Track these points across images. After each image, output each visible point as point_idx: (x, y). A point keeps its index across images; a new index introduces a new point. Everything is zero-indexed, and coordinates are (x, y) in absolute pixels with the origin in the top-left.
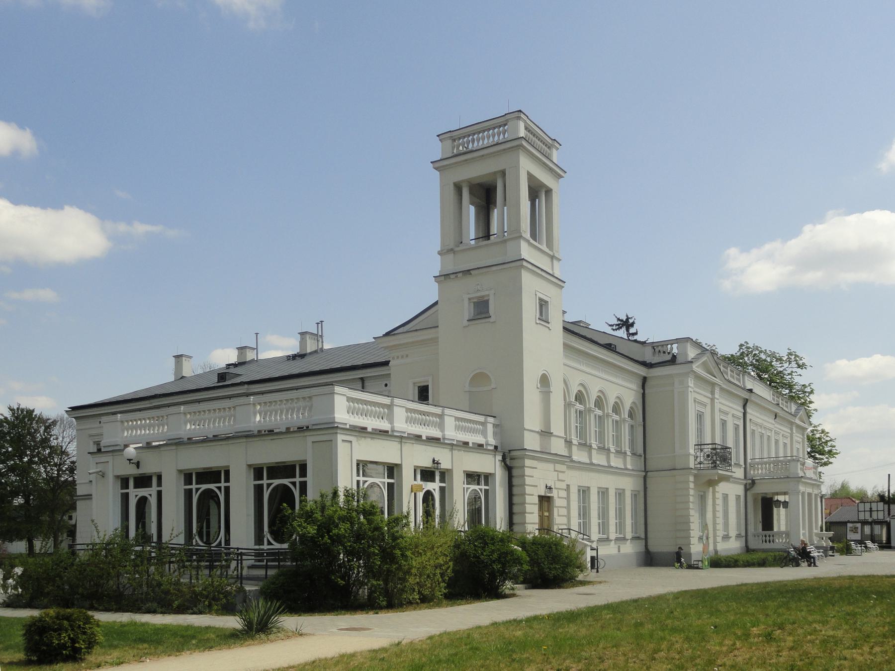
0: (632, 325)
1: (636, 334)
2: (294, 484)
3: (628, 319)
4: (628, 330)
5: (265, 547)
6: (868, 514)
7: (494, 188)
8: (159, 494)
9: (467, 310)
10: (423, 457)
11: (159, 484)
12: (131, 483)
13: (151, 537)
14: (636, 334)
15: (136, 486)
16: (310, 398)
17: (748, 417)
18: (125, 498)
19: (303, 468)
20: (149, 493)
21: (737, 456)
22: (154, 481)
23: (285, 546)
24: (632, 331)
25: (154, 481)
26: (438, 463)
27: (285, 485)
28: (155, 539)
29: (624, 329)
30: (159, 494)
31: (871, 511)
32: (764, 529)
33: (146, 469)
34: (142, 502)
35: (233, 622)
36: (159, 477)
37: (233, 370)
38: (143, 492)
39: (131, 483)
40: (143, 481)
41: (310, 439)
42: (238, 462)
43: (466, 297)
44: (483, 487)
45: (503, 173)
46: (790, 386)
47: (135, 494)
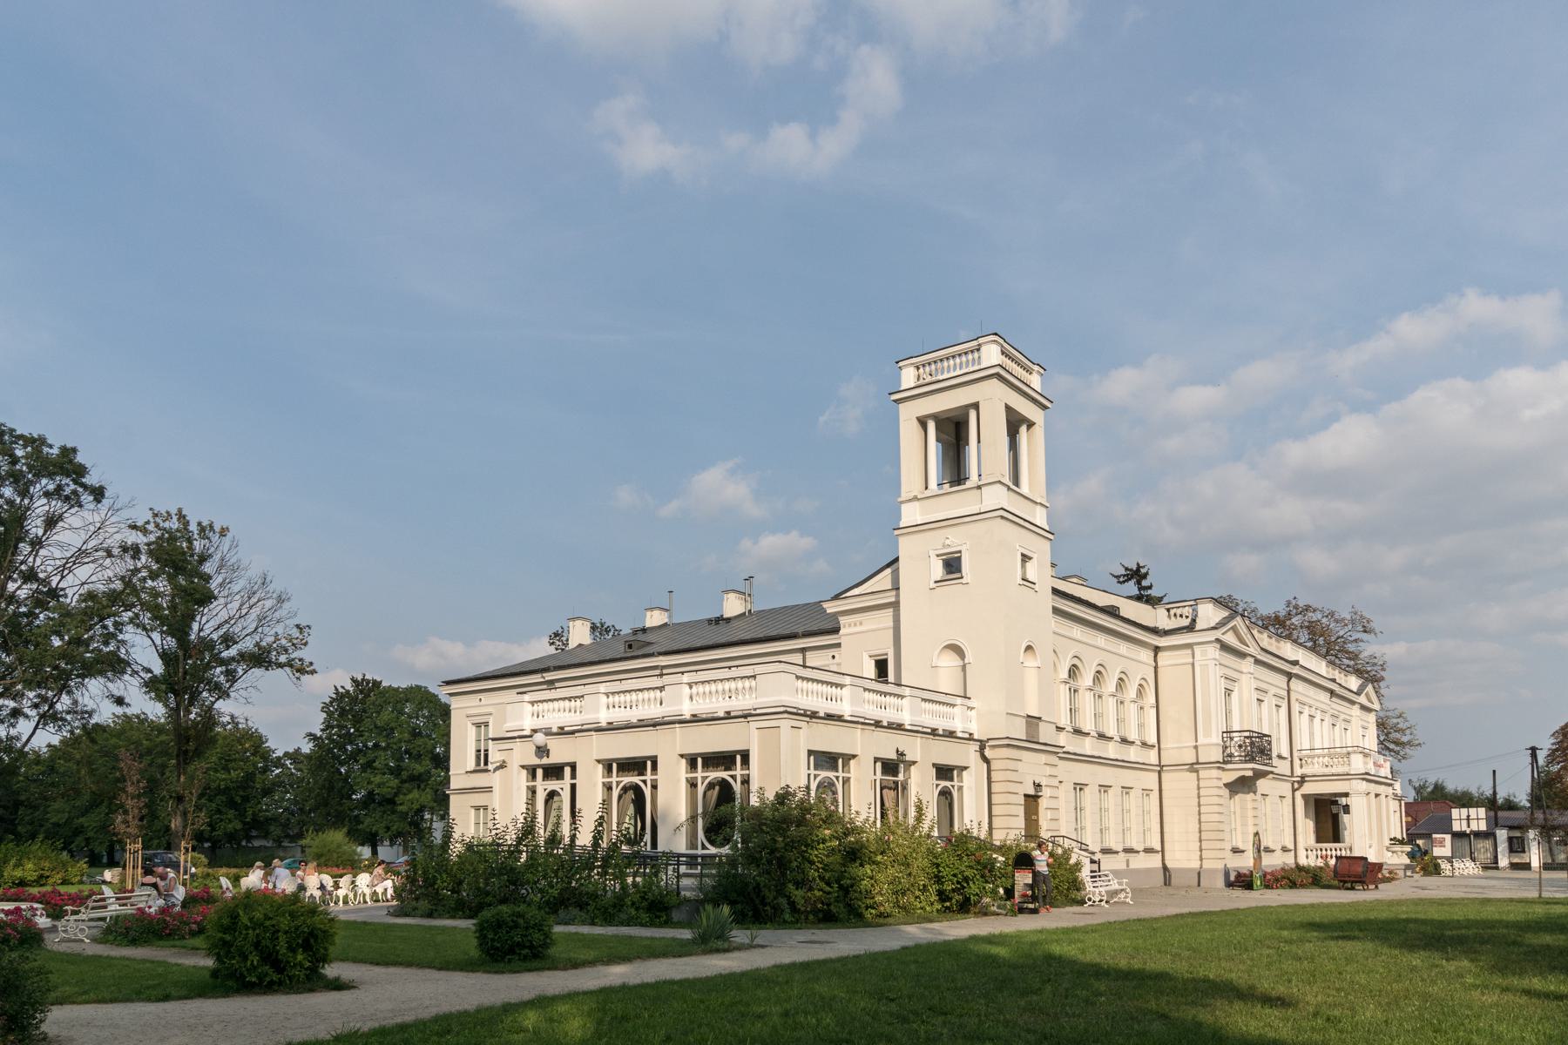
0: (1145, 576)
1: (1150, 587)
2: (704, 778)
3: (1139, 567)
4: (1139, 583)
5: (700, 852)
6: (1464, 823)
7: (967, 422)
8: (573, 787)
9: (938, 570)
10: (887, 746)
11: (573, 776)
12: (540, 772)
13: (562, 838)
14: (1150, 587)
15: (546, 776)
16: (754, 677)
17: (1293, 696)
18: (533, 791)
19: (745, 757)
20: (562, 786)
21: (1280, 746)
22: (567, 770)
23: (726, 850)
24: (1145, 583)
25: (567, 770)
26: (903, 754)
27: (724, 780)
28: (567, 840)
29: (1132, 582)
30: (573, 787)
31: (1468, 819)
32: (1318, 840)
33: (554, 758)
34: (552, 795)
35: (686, 934)
36: (573, 767)
37: (641, 637)
38: (553, 785)
39: (540, 772)
40: (554, 772)
41: (754, 725)
42: (669, 748)
43: (933, 554)
44: (840, 774)
45: (976, 406)
46: (1354, 656)
47: (543, 787)
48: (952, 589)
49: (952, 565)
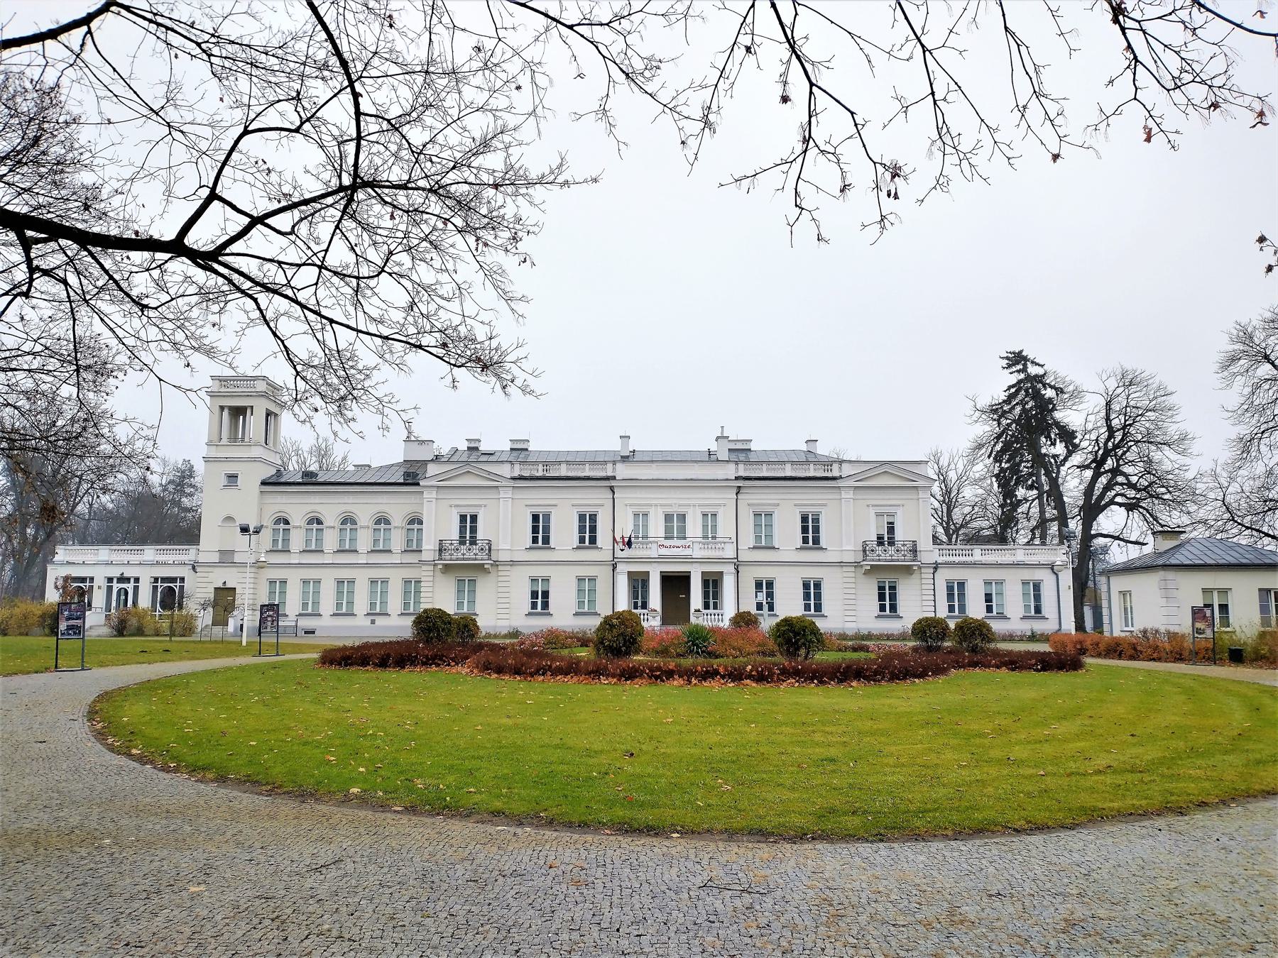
9: (224, 481)
48: (231, 492)
49: (233, 478)
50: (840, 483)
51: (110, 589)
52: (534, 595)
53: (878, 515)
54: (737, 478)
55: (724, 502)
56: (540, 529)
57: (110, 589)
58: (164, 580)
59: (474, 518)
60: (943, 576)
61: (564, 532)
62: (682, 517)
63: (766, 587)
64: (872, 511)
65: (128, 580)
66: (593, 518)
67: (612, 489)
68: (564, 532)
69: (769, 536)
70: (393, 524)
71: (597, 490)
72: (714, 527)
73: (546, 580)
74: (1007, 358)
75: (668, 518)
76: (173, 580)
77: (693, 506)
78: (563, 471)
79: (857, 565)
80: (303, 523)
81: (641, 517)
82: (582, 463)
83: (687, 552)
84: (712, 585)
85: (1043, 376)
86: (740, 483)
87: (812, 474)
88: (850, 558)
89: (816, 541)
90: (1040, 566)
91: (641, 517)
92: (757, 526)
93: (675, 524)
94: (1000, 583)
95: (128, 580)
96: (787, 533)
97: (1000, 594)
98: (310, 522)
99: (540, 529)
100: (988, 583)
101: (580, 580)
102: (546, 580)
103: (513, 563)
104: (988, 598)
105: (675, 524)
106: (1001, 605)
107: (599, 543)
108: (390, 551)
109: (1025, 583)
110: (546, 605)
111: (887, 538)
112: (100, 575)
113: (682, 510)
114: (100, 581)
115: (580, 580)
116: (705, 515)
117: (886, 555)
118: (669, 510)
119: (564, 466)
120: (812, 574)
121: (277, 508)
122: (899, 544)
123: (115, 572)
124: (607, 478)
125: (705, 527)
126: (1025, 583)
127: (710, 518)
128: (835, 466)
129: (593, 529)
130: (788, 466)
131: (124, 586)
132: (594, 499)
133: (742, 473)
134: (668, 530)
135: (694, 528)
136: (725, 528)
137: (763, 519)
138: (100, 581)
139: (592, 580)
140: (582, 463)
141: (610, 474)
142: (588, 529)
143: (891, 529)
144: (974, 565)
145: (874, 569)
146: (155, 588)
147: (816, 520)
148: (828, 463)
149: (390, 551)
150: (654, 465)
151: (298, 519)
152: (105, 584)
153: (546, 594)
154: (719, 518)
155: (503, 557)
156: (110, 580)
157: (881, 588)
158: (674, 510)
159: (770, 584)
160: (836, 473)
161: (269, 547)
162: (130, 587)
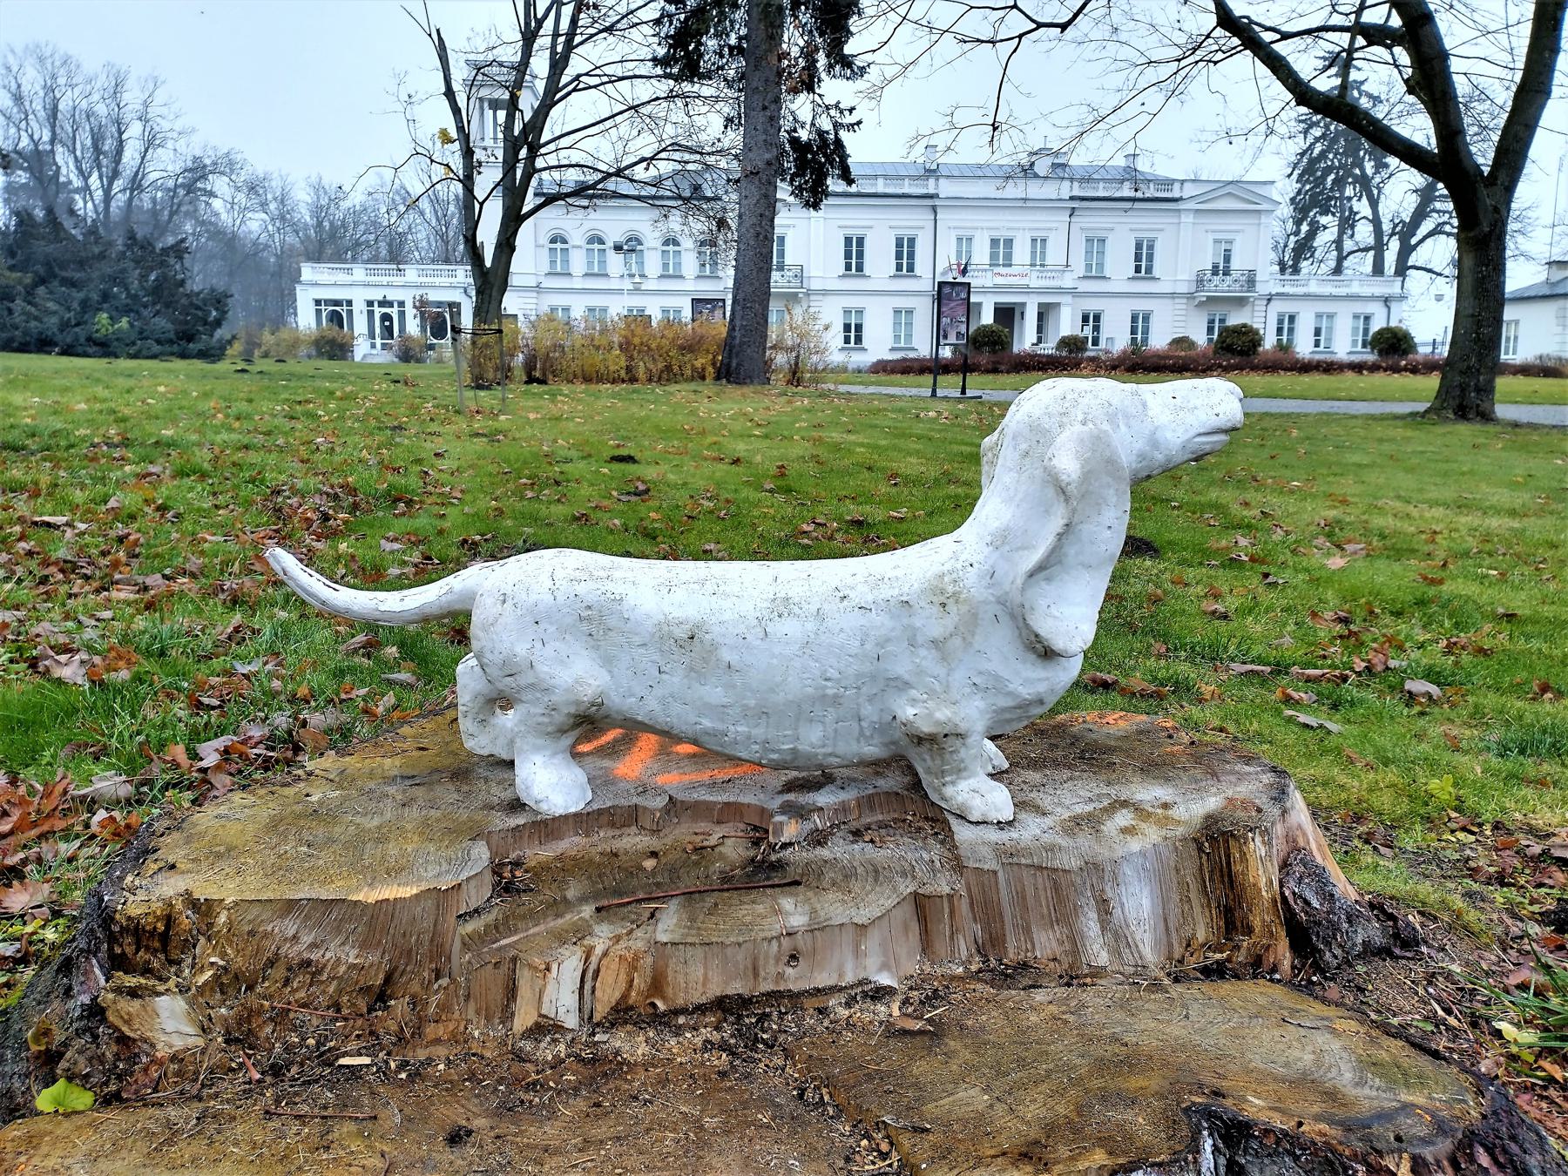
50: (1181, 205)
51: (371, 314)
52: (847, 328)
53: (1217, 241)
54: (1072, 198)
55: (1054, 225)
56: (854, 251)
57: (371, 314)
58: (328, 302)
59: (861, 241)
60: (1277, 307)
61: (880, 259)
62: (1009, 243)
63: (1093, 319)
64: (1211, 237)
65: (390, 304)
66: (912, 241)
67: (934, 209)
68: (880, 259)
69: (1101, 265)
70: (571, 242)
71: (919, 210)
72: (1043, 253)
73: (860, 312)
74: (1325, 59)
75: (994, 242)
76: (337, 303)
77: (1021, 229)
78: (881, 187)
79: (1190, 296)
80: (658, 244)
81: (964, 241)
82: (902, 178)
83: (1024, 281)
84: (1044, 313)
85: (1362, 83)
86: (1075, 204)
87: (906, 190)
88: (1183, 288)
89: (860, 268)
90: (1373, 298)
91: (964, 241)
92: (1089, 252)
93: (1002, 249)
94: (1331, 316)
95: (390, 304)
96: (1119, 262)
97: (1330, 329)
98: (591, 241)
99: (854, 251)
100: (1319, 316)
101: (897, 312)
102: (860, 312)
103: (825, 293)
104: (1318, 332)
105: (1002, 249)
106: (1329, 340)
107: (918, 271)
108: (681, 277)
109: (1356, 317)
110: (859, 339)
111: (1222, 269)
112: (359, 297)
113: (1009, 234)
114: (359, 309)
115: (897, 312)
116: (959, 239)
117: (1221, 286)
118: (996, 234)
119: (881, 181)
120: (1142, 305)
121: (554, 224)
122: (1235, 275)
123: (377, 295)
124: (931, 197)
125: (1033, 253)
126: (1356, 317)
127: (1039, 244)
128: (1177, 186)
129: (911, 255)
130: (881, 181)
131: (388, 310)
132: (913, 221)
133: (1077, 192)
134: (994, 256)
135: (1021, 253)
136: (1055, 255)
137: (1096, 245)
138: (359, 309)
139: (910, 312)
140: (902, 178)
141: (931, 191)
142: (905, 254)
143: (1227, 259)
144: (1307, 297)
145: (1211, 300)
146: (318, 312)
147: (1151, 247)
148: (1168, 183)
149: (681, 277)
150: (981, 182)
151: (577, 237)
152: (365, 309)
153: (859, 328)
154: (1049, 244)
155: (815, 285)
156: (370, 303)
157: (1211, 322)
158: (1002, 234)
159: (1097, 318)
160: (1176, 194)
161: (547, 270)
162: (394, 312)
